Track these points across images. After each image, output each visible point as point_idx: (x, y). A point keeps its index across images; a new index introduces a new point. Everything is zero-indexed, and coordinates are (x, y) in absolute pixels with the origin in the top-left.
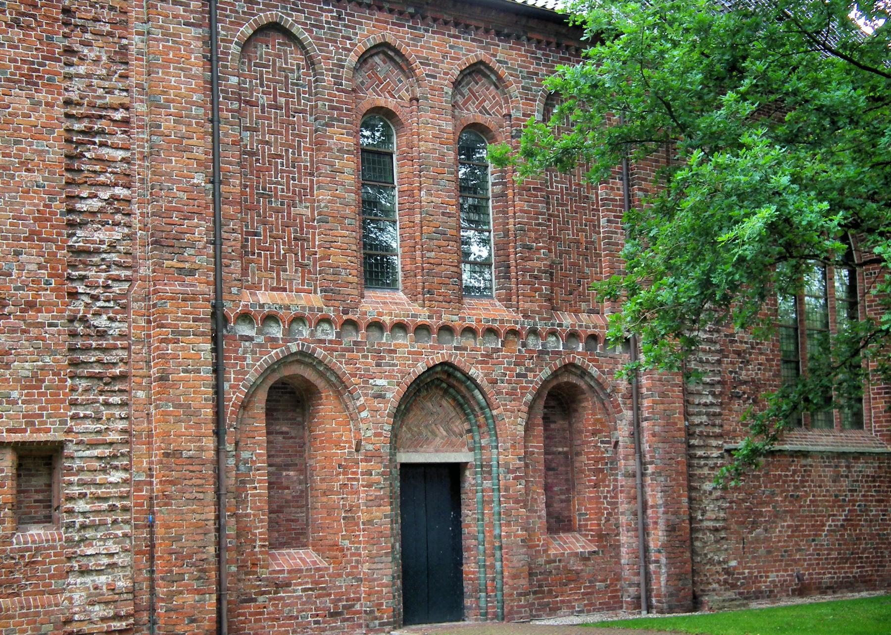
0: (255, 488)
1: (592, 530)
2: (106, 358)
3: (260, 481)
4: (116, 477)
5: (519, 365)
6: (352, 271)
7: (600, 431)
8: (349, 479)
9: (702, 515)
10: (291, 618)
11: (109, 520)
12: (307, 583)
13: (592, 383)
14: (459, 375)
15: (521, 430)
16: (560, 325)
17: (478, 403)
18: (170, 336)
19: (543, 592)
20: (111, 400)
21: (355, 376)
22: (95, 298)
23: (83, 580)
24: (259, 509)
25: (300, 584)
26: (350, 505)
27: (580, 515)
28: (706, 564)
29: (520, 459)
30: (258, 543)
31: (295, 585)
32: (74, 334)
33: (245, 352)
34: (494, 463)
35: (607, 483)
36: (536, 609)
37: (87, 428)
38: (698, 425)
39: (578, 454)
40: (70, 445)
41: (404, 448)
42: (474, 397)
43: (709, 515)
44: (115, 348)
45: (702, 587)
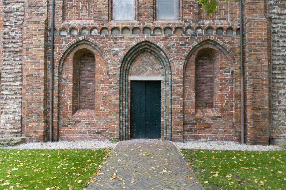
0: (68, 88)
1: (219, 108)
2: (14, 46)
3: (70, 86)
4: (17, 83)
5: (181, 41)
7: (224, 68)
8: (105, 85)
9: (279, 104)
10: (80, 133)
11: (15, 97)
13: (220, 48)
14: (153, 46)
15: (182, 67)
16: (203, 24)
18: (30, 36)
20: (16, 59)
21: (105, 47)
22: (12, 27)
23: (5, 116)
24: (69, 95)
25: (84, 122)
26: (105, 95)
27: (216, 101)
28: (279, 125)
29: (181, 78)
30: (69, 107)
31: (82, 122)
32: (5, 39)
33: (62, 41)
34: (170, 80)
35: (227, 89)
37: (8, 68)
38: (278, 64)
39: (215, 77)
40: (3, 73)
41: (133, 75)
42: (161, 55)
43: (282, 104)
44: (18, 42)
45: (277, 135)
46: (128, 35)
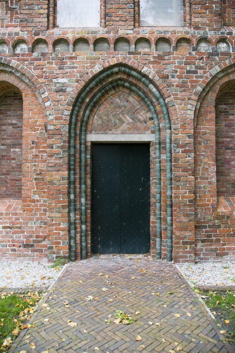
5: (189, 64)
6: (43, 6)
8: (40, 152)
12: (7, 223)
14: (134, 73)
15: (191, 114)
17: (155, 96)
19: (212, 241)
29: (189, 137)
34: (168, 140)
36: (204, 254)
46: (85, 53)
